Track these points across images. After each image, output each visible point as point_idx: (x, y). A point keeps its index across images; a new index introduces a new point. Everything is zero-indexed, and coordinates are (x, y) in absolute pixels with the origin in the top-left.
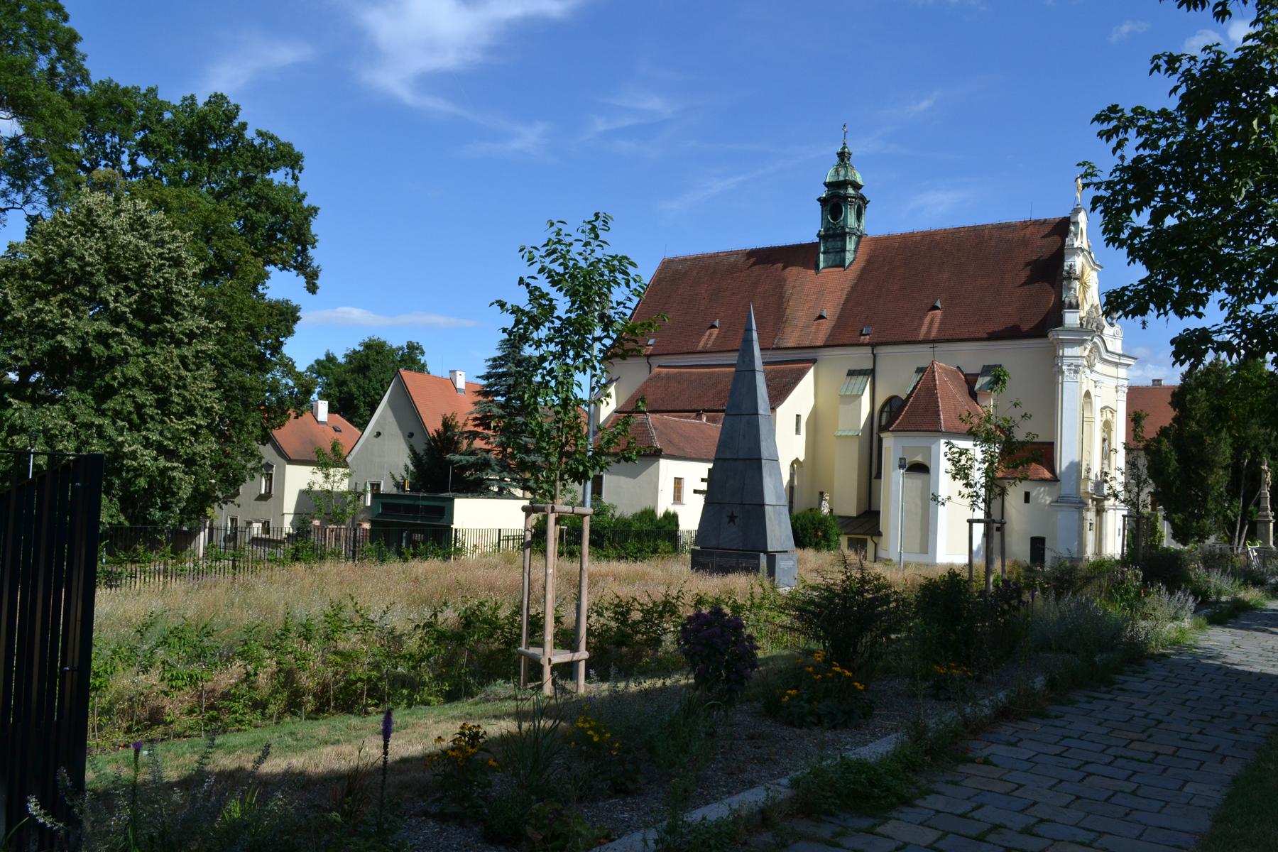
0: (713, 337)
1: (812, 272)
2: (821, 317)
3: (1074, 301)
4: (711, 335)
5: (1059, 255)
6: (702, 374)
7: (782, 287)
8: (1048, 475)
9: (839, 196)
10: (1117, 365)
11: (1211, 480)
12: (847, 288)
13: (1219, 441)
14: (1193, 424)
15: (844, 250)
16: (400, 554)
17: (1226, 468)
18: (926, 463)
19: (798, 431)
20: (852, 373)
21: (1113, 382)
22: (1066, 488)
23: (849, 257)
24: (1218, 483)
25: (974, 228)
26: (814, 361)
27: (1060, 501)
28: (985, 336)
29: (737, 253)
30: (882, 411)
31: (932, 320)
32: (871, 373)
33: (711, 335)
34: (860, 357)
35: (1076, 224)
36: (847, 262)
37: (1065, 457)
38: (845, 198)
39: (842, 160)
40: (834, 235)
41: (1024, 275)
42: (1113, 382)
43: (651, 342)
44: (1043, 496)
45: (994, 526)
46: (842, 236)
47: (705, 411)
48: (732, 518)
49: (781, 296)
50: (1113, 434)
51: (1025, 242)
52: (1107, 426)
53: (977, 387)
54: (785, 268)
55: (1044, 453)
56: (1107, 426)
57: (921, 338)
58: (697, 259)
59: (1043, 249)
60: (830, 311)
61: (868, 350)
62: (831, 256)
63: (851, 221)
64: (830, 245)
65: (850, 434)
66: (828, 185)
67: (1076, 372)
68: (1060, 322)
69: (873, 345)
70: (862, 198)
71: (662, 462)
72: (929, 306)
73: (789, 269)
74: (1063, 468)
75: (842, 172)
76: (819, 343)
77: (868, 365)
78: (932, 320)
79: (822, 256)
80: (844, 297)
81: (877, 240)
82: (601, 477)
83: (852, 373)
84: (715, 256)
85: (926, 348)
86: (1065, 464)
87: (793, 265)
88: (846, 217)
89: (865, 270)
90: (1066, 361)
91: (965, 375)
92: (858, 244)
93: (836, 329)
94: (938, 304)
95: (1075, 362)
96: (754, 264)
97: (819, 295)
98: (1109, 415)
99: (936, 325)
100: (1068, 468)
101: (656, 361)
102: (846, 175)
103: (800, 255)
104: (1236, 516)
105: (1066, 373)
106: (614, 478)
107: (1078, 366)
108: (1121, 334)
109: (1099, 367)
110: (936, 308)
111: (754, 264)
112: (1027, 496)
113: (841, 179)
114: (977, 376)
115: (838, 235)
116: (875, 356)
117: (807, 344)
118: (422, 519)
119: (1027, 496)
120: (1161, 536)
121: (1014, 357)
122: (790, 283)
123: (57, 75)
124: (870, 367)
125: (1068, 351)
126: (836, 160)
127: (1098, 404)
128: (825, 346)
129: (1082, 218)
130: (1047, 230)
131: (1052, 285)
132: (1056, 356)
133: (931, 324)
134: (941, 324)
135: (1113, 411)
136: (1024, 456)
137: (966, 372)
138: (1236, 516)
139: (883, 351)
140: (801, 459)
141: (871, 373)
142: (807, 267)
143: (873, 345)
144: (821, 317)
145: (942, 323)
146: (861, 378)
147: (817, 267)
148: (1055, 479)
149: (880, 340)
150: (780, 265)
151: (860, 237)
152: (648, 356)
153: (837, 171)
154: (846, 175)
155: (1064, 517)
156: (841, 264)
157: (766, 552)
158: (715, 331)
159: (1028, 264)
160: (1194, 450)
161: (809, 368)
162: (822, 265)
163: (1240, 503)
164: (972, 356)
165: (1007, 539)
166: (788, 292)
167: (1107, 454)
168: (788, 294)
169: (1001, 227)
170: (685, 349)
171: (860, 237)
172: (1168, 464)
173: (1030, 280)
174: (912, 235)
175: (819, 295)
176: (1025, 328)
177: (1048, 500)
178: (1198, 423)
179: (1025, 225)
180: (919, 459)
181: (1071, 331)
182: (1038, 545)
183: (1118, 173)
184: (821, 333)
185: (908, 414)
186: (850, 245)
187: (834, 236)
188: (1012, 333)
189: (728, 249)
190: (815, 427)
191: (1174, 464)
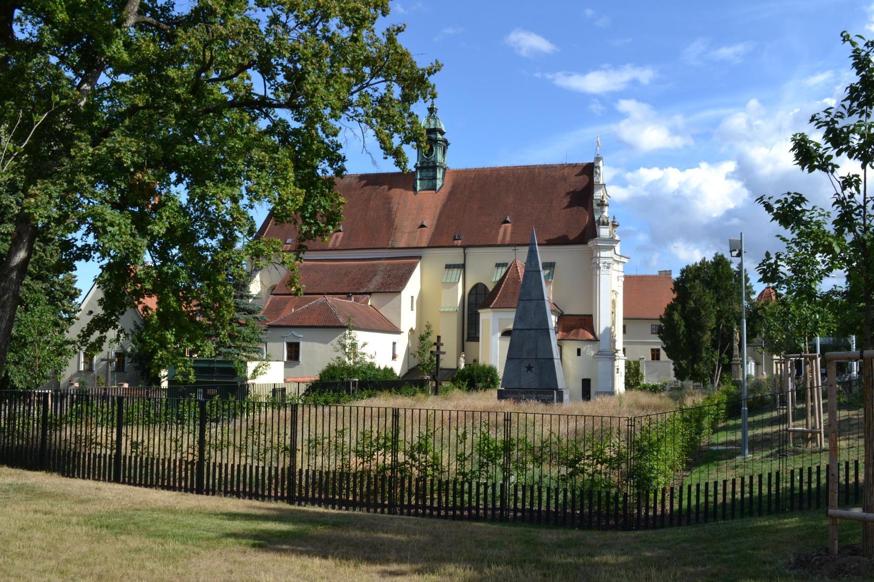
0: (340, 239)
1: (411, 193)
2: (423, 226)
3: (606, 221)
4: (337, 237)
5: (590, 187)
6: (333, 266)
7: (390, 204)
8: (591, 337)
12: (440, 206)
15: (435, 178)
16: (390, 391)
19: (412, 310)
20: (448, 267)
22: (603, 345)
23: (439, 183)
26: (420, 258)
27: (600, 354)
28: (544, 242)
30: (470, 293)
32: (463, 267)
33: (337, 237)
34: (454, 256)
41: (566, 201)
44: (589, 350)
46: (434, 168)
47: (354, 294)
48: (529, 368)
49: (390, 210)
51: (564, 179)
54: (390, 189)
57: (499, 243)
59: (581, 182)
60: (429, 221)
61: (461, 250)
62: (426, 182)
63: (439, 158)
64: (424, 174)
65: (451, 310)
67: (608, 268)
68: (594, 234)
70: (446, 141)
72: (502, 221)
73: (393, 190)
74: (601, 331)
75: (432, 122)
76: (423, 245)
77: (460, 261)
79: (418, 182)
81: (458, 172)
82: (297, 345)
83: (448, 267)
85: (510, 250)
86: (602, 329)
87: (400, 187)
88: (436, 154)
90: (602, 260)
94: (508, 219)
96: (365, 185)
97: (418, 209)
102: (435, 124)
106: (309, 344)
110: (507, 222)
111: (365, 185)
112: (579, 351)
113: (432, 127)
115: (431, 167)
117: (415, 245)
118: (217, 377)
119: (579, 351)
120: (642, 376)
122: (395, 200)
123: (220, 115)
124: (462, 262)
125: (603, 254)
126: (427, 113)
128: (428, 247)
130: (578, 171)
133: (505, 233)
135: (616, 293)
139: (470, 251)
142: (407, 189)
143: (464, 247)
144: (423, 226)
145: (513, 233)
146: (455, 270)
147: (415, 189)
148: (596, 340)
149: (469, 243)
150: (386, 187)
151: (445, 169)
153: (428, 120)
154: (435, 124)
155: (602, 364)
156: (433, 188)
157: (557, 389)
158: (341, 234)
159: (568, 194)
161: (417, 263)
162: (418, 188)
163: (717, 353)
169: (546, 167)
173: (570, 205)
174: (483, 170)
176: (571, 237)
177: (593, 353)
181: (605, 240)
183: (291, 15)
184: (425, 238)
186: (439, 175)
187: (427, 168)
188: (562, 241)
190: (422, 305)
191: (682, 328)
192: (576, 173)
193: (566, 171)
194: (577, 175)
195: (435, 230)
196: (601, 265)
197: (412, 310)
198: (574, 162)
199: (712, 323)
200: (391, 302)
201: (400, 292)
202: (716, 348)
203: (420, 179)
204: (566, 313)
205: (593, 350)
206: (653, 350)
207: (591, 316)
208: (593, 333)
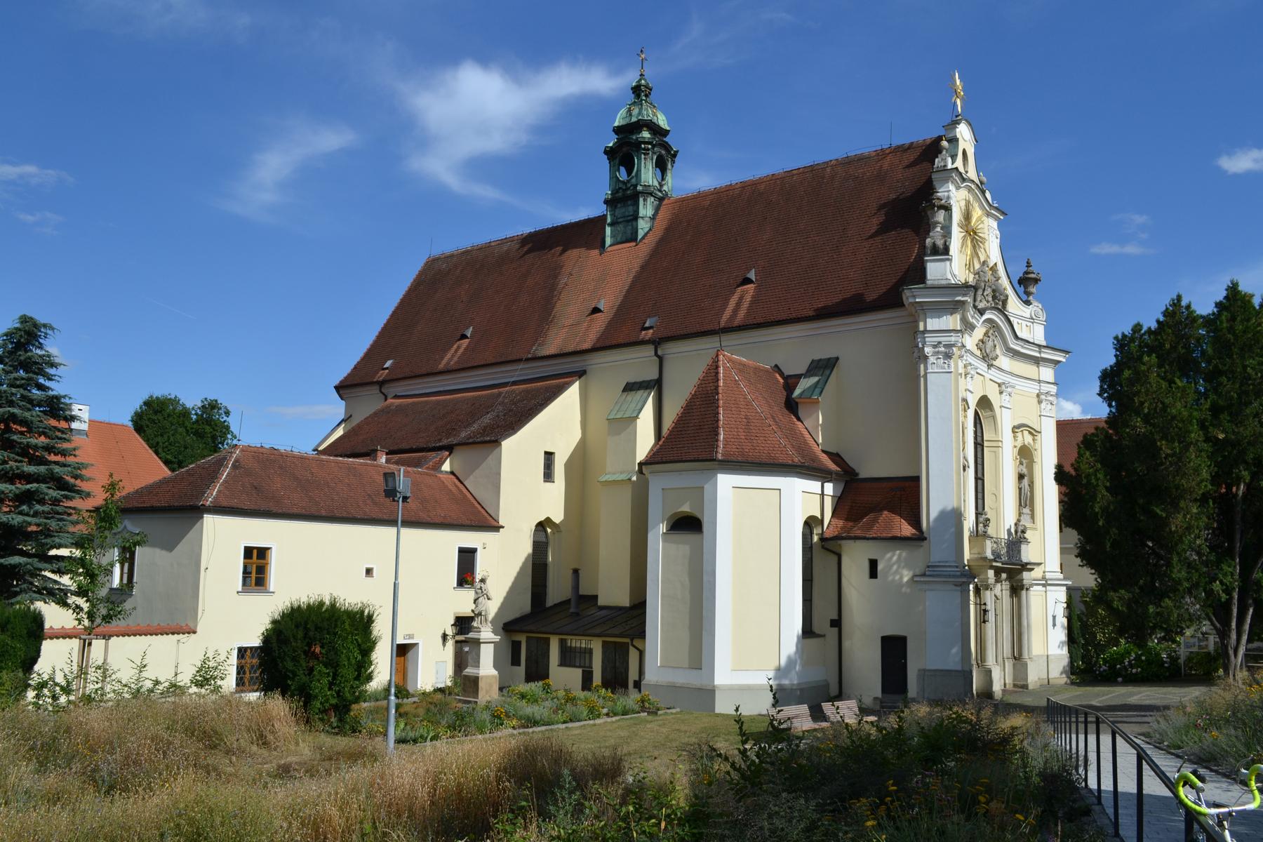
1: (597, 252)
2: (596, 310)
6: (438, 402)
8: (907, 530)
9: (629, 144)
10: (1037, 361)
11: (1177, 523)
12: (636, 267)
13: (1187, 448)
14: (1138, 422)
15: (636, 217)
17: (1203, 500)
18: (698, 515)
19: (548, 476)
20: (630, 388)
21: (1033, 388)
22: (937, 552)
23: (643, 226)
24: (1189, 528)
25: (812, 169)
26: (581, 374)
27: (930, 575)
28: (811, 313)
29: (511, 239)
31: (741, 298)
32: (656, 385)
34: (639, 363)
35: (954, 141)
36: (641, 234)
37: (935, 502)
38: (637, 145)
39: (638, 96)
40: (624, 198)
42: (1033, 388)
43: (388, 364)
44: (899, 568)
45: (822, 619)
50: (1037, 468)
52: (1025, 454)
53: (797, 392)
54: (564, 251)
55: (904, 494)
56: (1025, 454)
58: (467, 252)
61: (648, 351)
62: (620, 227)
63: (648, 174)
64: (619, 212)
66: (618, 130)
67: (948, 356)
69: (657, 343)
71: (209, 520)
72: (740, 280)
75: (635, 111)
76: (587, 346)
78: (741, 298)
79: (608, 230)
80: (630, 280)
84: (488, 246)
87: (576, 247)
89: (662, 242)
90: (930, 339)
91: (786, 378)
92: (657, 209)
93: (612, 325)
94: (752, 275)
95: (945, 339)
96: (527, 253)
97: (598, 283)
98: (1028, 439)
99: (745, 305)
100: (937, 519)
101: (392, 389)
103: (583, 234)
104: (1228, 591)
105: (932, 359)
107: (949, 346)
108: (1043, 316)
109: (1004, 361)
111: (527, 253)
112: (873, 564)
114: (799, 377)
116: (661, 359)
119: (873, 564)
121: (855, 342)
124: (654, 375)
125: (933, 323)
127: (1006, 420)
128: (594, 350)
129: (963, 132)
130: (912, 156)
131: (917, 232)
132: (916, 332)
133: (738, 305)
134: (752, 303)
135: (1034, 433)
136: (877, 502)
137: (786, 373)
138: (1228, 591)
139: (671, 349)
140: (558, 517)
141: (656, 385)
143: (657, 343)
144: (596, 310)
145: (755, 301)
146: (640, 392)
150: (560, 249)
152: (381, 384)
155: (937, 601)
156: (633, 238)
160: (1140, 468)
162: (608, 241)
164: (792, 348)
165: (846, 644)
166: (563, 280)
167: (1026, 500)
168: (561, 286)
169: (848, 162)
170: (424, 371)
171: (661, 200)
172: (1093, 498)
173: (884, 229)
175: (598, 283)
176: (871, 296)
177: (906, 576)
178: (1147, 420)
179: (882, 154)
180: (686, 508)
182: (894, 650)
185: (694, 443)
186: (646, 209)
188: (853, 307)
189: (501, 236)
192: (906, 162)
193: (886, 164)
194: (908, 167)
195: (616, 314)
196: (928, 350)
197: (548, 476)
198: (905, 140)
199: (1199, 470)
200: (484, 465)
201: (496, 443)
202: (1230, 553)
203: (611, 225)
204: (864, 474)
205: (908, 566)
206: (462, 551)
207: (917, 479)
208: (915, 521)
